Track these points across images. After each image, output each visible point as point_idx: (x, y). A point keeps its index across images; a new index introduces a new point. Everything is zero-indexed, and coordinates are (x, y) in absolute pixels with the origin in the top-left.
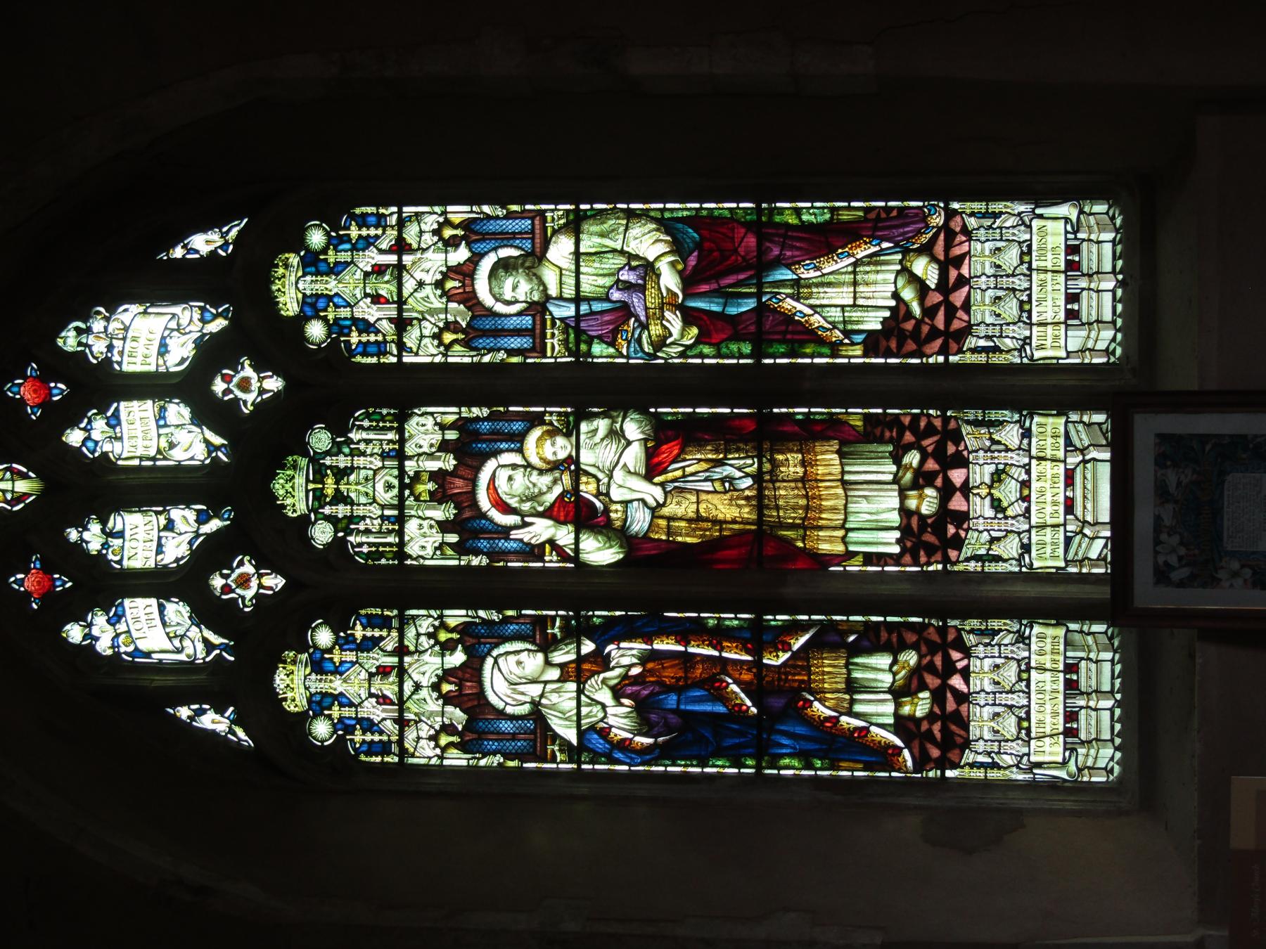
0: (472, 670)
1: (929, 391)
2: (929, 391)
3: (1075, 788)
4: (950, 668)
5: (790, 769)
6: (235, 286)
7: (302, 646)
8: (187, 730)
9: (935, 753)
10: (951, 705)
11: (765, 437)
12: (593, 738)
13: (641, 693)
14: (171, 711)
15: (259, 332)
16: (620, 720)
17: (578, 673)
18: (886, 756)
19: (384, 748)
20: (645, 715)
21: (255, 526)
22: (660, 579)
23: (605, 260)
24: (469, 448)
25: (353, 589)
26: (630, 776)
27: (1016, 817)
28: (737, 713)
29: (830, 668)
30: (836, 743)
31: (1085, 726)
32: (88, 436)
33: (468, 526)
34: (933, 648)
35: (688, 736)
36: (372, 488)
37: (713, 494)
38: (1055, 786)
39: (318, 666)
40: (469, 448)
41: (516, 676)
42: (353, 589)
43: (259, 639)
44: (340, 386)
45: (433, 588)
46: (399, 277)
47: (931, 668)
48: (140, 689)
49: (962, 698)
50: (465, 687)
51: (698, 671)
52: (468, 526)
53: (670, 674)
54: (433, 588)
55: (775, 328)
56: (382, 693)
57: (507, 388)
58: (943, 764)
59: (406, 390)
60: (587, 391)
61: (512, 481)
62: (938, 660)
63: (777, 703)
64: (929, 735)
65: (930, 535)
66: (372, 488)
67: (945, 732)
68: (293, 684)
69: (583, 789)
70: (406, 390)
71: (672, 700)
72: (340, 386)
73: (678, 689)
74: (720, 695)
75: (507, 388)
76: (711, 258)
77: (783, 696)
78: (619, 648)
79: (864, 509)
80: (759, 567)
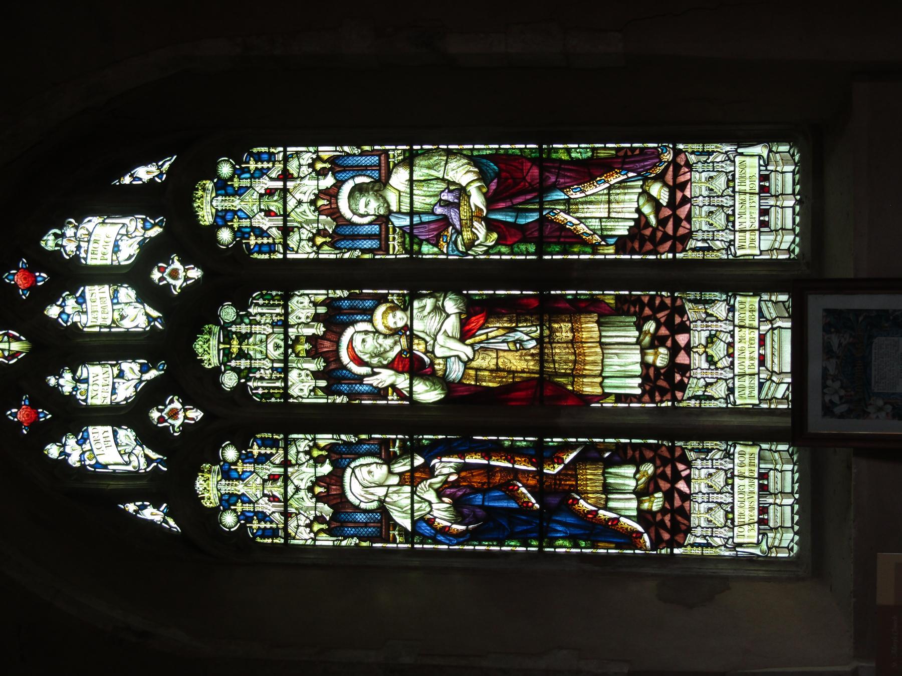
0: (336, 477)
1: (662, 278)
2: (662, 278)
3: (766, 561)
4: (677, 476)
5: (563, 548)
6: (168, 203)
7: (215, 460)
8: (133, 520)
9: (666, 536)
10: (677, 502)
11: (545, 312)
12: (423, 526)
13: (457, 494)
14: (122, 507)
15: (184, 237)
16: (442, 513)
17: (411, 479)
18: (631, 539)
19: (274, 533)
20: (459, 509)
21: (181, 375)
22: (470, 413)
23: (431, 185)
24: (334, 319)
25: (251, 420)
26: (449, 552)
27: (724, 582)
28: (525, 508)
29: (591, 476)
30: (596, 529)
31: (773, 517)
32: (63, 310)
33: (333, 375)
34: (665, 462)
35: (490, 524)
36: (265, 347)
37: (508, 352)
38: (751, 560)
39: (227, 475)
40: (334, 319)
41: (368, 482)
42: (251, 420)
43: (185, 456)
44: (242, 275)
45: (308, 419)
46: (285, 198)
47: (663, 476)
48: (99, 491)
49: (686, 497)
50: (331, 490)
51: (498, 478)
52: (333, 375)
53: (478, 480)
54: (308, 419)
55: (552, 234)
56: (272, 493)
57: (362, 276)
58: (672, 544)
59: (289, 277)
60: (418, 279)
61: (365, 343)
62: (668, 470)
63: (554, 500)
64: (662, 524)
65: (663, 381)
66: (265, 347)
67: (674, 522)
68: (209, 487)
69: (416, 562)
70: (289, 277)
71: (478, 499)
72: (242, 275)
73: (483, 491)
74: (513, 495)
75: (362, 276)
76: (507, 184)
77: (558, 496)
78: (441, 462)
79: (616, 362)
80: (541, 404)
